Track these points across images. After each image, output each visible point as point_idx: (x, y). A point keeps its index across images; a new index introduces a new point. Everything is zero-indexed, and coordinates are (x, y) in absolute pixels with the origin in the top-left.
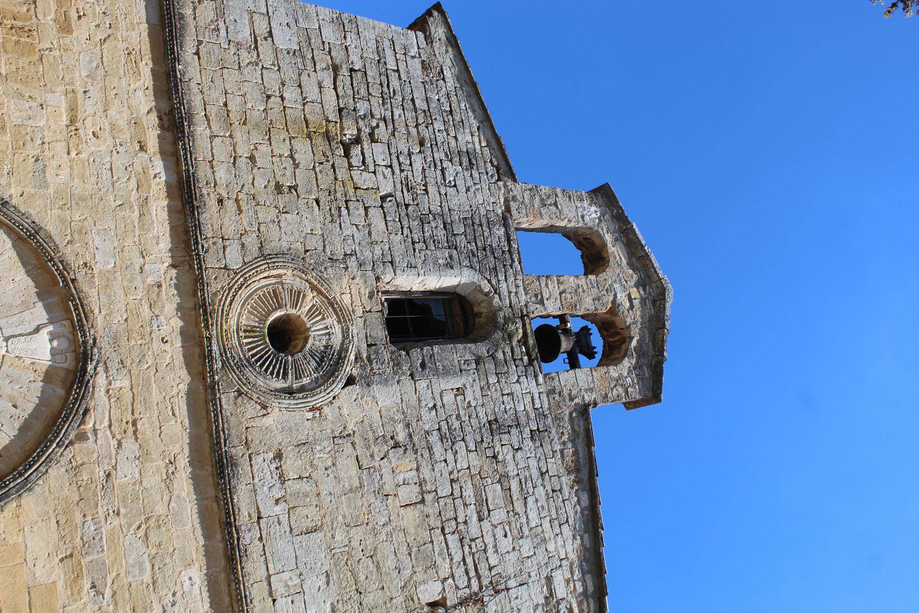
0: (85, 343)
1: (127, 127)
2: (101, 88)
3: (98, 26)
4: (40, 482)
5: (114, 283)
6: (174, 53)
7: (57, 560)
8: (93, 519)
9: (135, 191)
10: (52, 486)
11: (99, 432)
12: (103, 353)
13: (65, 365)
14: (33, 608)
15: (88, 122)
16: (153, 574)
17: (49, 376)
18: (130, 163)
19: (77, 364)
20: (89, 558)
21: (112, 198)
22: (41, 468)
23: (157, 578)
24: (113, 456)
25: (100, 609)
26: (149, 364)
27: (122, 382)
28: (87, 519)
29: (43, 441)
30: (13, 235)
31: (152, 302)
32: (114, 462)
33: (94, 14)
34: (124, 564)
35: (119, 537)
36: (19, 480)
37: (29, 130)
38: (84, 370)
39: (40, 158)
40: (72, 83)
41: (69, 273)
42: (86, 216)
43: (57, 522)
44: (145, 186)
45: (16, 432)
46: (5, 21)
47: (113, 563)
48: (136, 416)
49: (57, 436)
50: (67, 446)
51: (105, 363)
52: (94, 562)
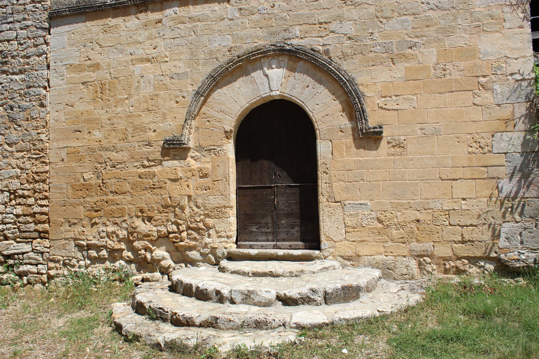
0: (274, 50)
1: (148, 31)
2: (127, 46)
3: (92, 49)
4: (350, 74)
5: (239, 35)
6: (100, 6)
7: (393, 66)
8: (373, 47)
9: (185, 25)
10: (353, 68)
11: (324, 43)
12: (280, 41)
13: (286, 61)
14: (417, 79)
15: (148, 52)
16: (410, 15)
17: (292, 70)
18: (169, 28)
19: (286, 55)
20: (395, 50)
21: (190, 38)
22: (342, 73)
23: (412, 12)
24: (339, 35)
25: (424, 45)
26: (286, 15)
27: (297, 31)
28: (373, 50)
29: (327, 72)
30: (215, 88)
31: (250, 13)
32: (342, 35)
33: (86, 52)
34: (401, 31)
35: (385, 33)
36: (348, 84)
37: (156, 82)
38: (289, 51)
39: (171, 76)
40: (127, 62)
41: (235, 60)
42: (201, 51)
43: (373, 66)
44: (182, 19)
45: (322, 86)
46: (99, 96)
47: (399, 37)
48: (316, 22)
49: (326, 65)
50: (332, 60)
51: (286, 39)
52: (397, 47)
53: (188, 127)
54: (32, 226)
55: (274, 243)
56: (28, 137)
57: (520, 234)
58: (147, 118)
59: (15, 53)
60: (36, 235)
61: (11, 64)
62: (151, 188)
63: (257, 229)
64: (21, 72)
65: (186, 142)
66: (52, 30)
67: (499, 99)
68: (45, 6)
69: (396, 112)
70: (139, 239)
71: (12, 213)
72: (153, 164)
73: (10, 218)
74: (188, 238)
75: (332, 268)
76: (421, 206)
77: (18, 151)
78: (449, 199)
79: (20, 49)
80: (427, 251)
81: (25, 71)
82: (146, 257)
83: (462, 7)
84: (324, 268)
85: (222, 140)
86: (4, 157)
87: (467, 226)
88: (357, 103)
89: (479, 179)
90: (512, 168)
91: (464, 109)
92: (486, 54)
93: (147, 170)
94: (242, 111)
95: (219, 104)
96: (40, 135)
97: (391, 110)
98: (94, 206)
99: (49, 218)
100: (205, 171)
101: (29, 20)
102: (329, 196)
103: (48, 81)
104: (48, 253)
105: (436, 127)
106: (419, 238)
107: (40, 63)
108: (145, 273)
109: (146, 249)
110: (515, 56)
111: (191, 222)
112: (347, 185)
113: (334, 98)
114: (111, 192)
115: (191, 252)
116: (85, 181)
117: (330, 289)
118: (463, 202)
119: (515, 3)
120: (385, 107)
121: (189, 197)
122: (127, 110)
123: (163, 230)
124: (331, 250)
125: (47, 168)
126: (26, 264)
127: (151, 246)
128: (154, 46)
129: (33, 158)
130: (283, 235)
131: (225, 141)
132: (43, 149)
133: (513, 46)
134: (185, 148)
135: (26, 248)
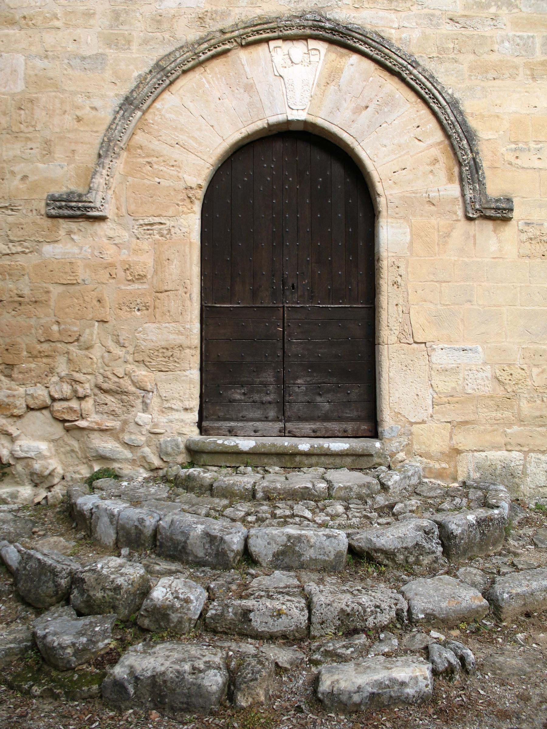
63: (244, 394)
65: (98, 205)
74: (97, 412)
85: (178, 205)
97: (527, 168)
100: (139, 270)
117: (458, 525)
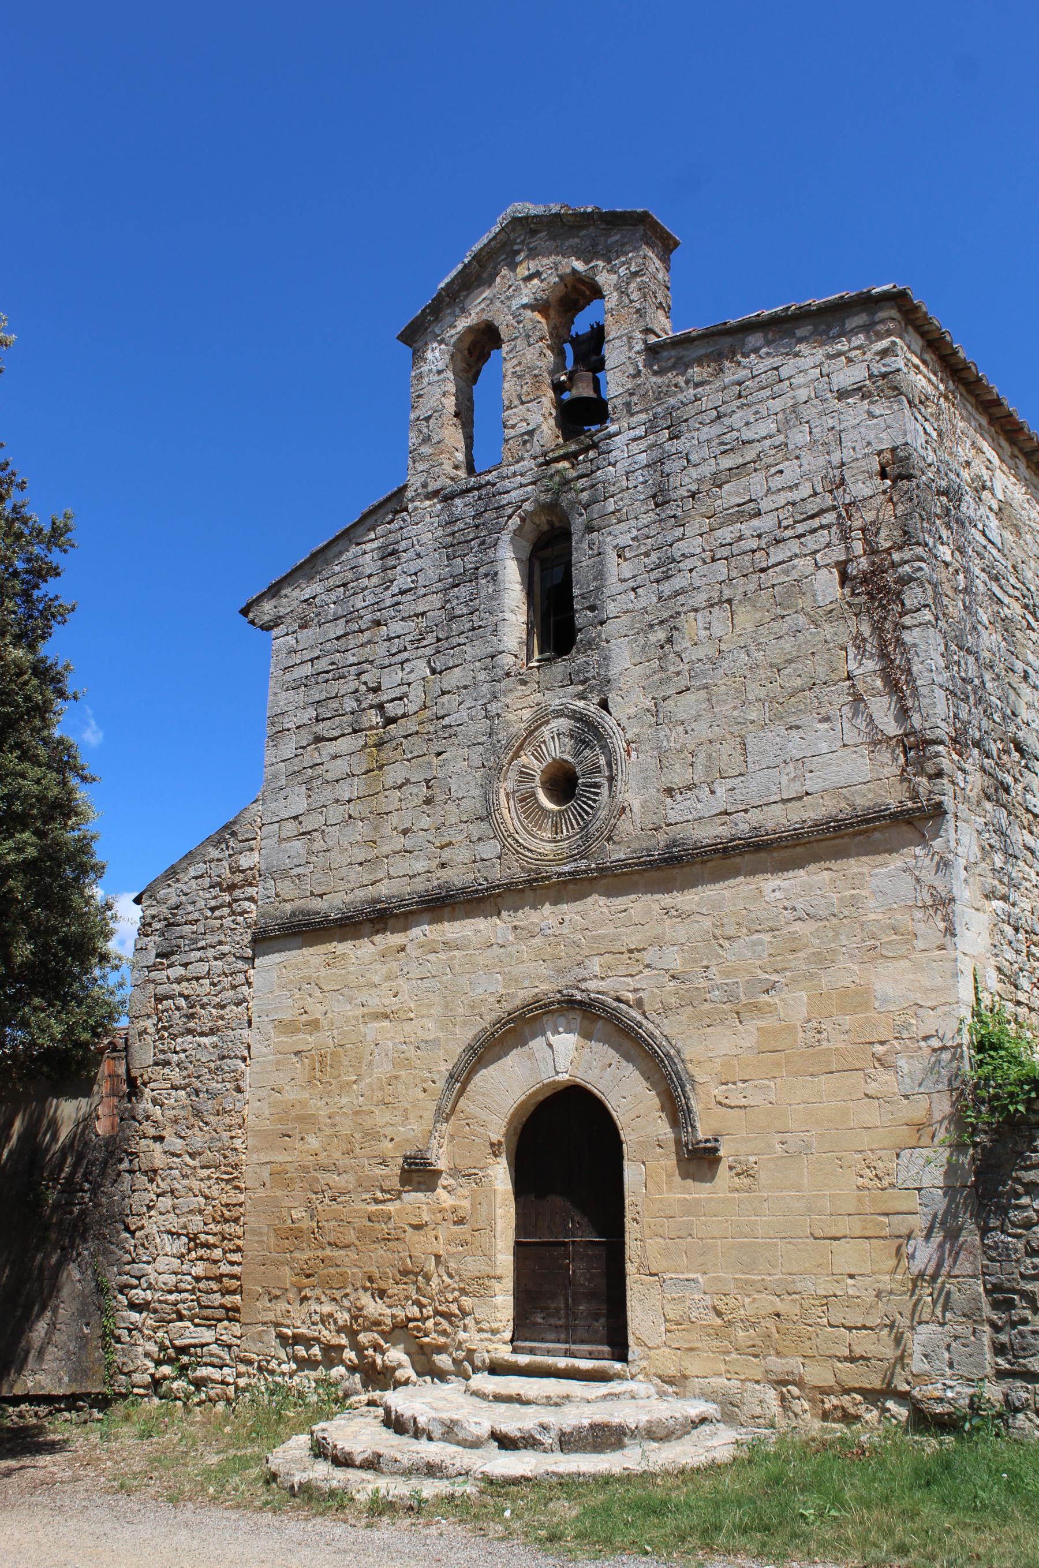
0: (559, 1002)
13: (579, 1020)
15: (386, 1001)
20: (742, 997)
32: (662, 972)
33: (301, 999)
37: (396, 1055)
40: (356, 1018)
45: (631, 1065)
48: (624, 950)
53: (437, 1134)
54: (217, 1299)
55: (567, 1346)
56: (217, 1143)
57: (948, 1348)
58: (381, 1118)
59: (205, 1000)
60: (221, 1313)
61: (200, 1019)
62: (385, 1239)
63: (543, 1318)
64: (212, 1032)
65: (432, 1161)
66: (256, 960)
67: (908, 1083)
68: (249, 920)
69: (742, 1112)
70: (367, 1329)
71: (190, 1274)
72: (389, 1196)
73: (186, 1284)
74: (436, 1331)
75: (627, 1396)
76: (783, 1286)
77: (202, 1167)
78: (828, 1275)
79: (213, 993)
80: (792, 1373)
81: (218, 1031)
82: (374, 1361)
83: (847, 913)
84: (610, 1394)
86: (183, 1176)
87: (857, 1328)
88: (679, 1096)
89: (876, 1238)
90: (930, 1218)
91: (851, 1104)
92: (885, 1000)
93: (380, 1207)
94: (516, 1109)
95: (484, 1095)
96: (234, 1140)
98: (305, 1266)
99: (241, 1285)
101: (226, 943)
102: (641, 1263)
103: (249, 1047)
104: (238, 1346)
105: (805, 1138)
106: (780, 1349)
107: (239, 1016)
108: (374, 1391)
109: (377, 1348)
110: (930, 1004)
111: (439, 1301)
112: (667, 1244)
113: (648, 1085)
114: (330, 1244)
115: (440, 1357)
116: (293, 1222)
118: (850, 1281)
119: (931, 903)
120: (726, 1101)
121: (438, 1257)
122: (355, 1102)
123: (401, 1314)
124: (644, 1363)
125: (242, 1198)
126: (206, 1364)
127: (382, 1342)
128: (394, 991)
129: (222, 1180)
130: (581, 1333)
131: (491, 1160)
132: (236, 1165)
133: (928, 984)
134: (434, 1171)
135: (207, 1335)
